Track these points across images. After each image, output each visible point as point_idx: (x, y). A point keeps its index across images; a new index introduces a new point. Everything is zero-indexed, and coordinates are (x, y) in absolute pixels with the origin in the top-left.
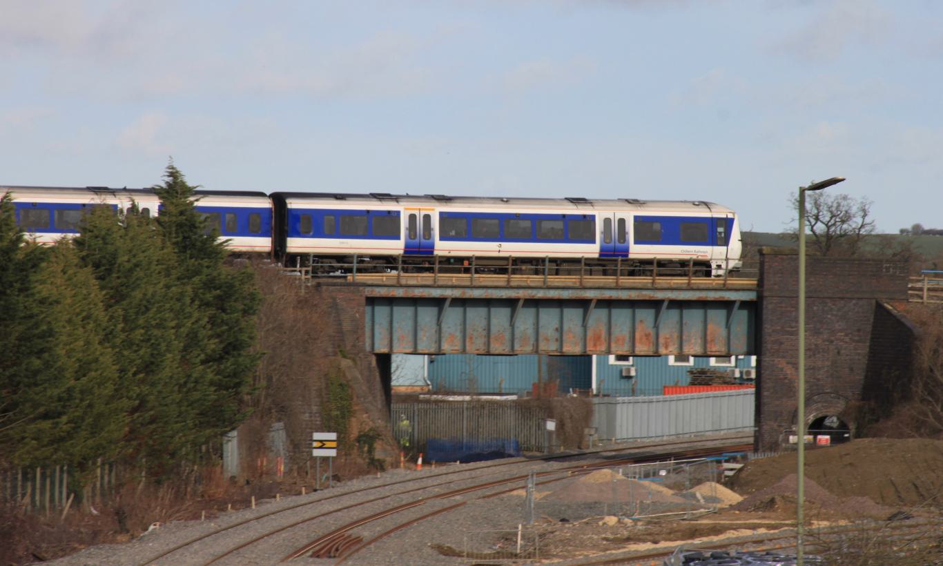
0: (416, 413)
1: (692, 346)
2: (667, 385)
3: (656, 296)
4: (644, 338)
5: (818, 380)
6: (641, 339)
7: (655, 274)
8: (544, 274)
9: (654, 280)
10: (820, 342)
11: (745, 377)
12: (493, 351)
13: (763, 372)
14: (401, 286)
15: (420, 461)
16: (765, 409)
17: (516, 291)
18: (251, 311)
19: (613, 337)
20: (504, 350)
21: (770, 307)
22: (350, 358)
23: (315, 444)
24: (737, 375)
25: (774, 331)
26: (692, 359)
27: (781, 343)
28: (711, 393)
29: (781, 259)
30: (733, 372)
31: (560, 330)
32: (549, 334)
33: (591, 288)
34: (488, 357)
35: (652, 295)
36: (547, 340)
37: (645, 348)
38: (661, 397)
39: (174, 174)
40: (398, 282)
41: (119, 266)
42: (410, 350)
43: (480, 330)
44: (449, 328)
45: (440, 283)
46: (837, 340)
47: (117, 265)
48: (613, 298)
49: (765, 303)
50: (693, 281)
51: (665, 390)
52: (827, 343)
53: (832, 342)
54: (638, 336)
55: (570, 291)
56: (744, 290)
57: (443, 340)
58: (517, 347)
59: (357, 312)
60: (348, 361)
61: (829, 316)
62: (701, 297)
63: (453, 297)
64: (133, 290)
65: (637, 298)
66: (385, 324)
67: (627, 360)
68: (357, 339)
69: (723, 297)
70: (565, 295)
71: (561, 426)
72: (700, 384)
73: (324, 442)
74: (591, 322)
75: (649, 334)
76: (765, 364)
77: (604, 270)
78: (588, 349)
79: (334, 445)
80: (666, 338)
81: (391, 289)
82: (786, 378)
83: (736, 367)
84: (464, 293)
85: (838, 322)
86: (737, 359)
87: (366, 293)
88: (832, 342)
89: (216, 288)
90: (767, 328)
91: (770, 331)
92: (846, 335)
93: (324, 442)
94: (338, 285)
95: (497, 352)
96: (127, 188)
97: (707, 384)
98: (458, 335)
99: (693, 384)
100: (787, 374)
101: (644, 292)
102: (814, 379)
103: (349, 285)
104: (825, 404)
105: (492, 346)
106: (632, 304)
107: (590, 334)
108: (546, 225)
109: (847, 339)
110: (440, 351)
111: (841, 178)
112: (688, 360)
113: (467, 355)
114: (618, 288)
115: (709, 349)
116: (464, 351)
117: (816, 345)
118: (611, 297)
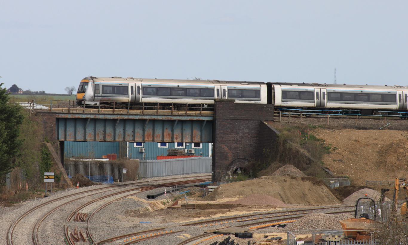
0: (70, 165)
2: (158, 156)
3: (144, 118)
5: (238, 153)
6: (166, 136)
7: (143, 109)
8: (157, 109)
10: (238, 137)
13: (215, 149)
15: (78, 185)
17: (117, 116)
18: (20, 123)
19: (155, 135)
20: (111, 140)
22: (50, 143)
23: (45, 177)
24: (186, 152)
25: (220, 133)
26: (167, 144)
27: (223, 138)
28: (177, 159)
30: (184, 151)
32: (130, 133)
35: (171, 118)
36: (129, 136)
37: (168, 140)
40: (69, 112)
43: (102, 132)
46: (245, 136)
49: (216, 121)
50: (188, 112)
57: (87, 136)
58: (117, 139)
59: (52, 124)
61: (242, 127)
62: (191, 119)
63: (91, 118)
68: (52, 135)
69: (200, 119)
70: (136, 117)
73: (49, 177)
75: (170, 134)
76: (217, 146)
77: (127, 107)
78: (145, 140)
79: (53, 177)
80: (177, 136)
81: (66, 115)
82: (225, 152)
83: (186, 148)
84: (96, 116)
87: (56, 116)
89: (5, 113)
90: (218, 132)
91: (219, 133)
92: (249, 135)
93: (49, 177)
95: (109, 141)
96: (246, 81)
99: (169, 155)
100: (225, 150)
101: (168, 117)
102: (236, 152)
105: (106, 138)
106: (163, 121)
108: (191, 91)
110: (85, 140)
113: (97, 142)
114: (157, 115)
116: (95, 140)
118: (155, 118)
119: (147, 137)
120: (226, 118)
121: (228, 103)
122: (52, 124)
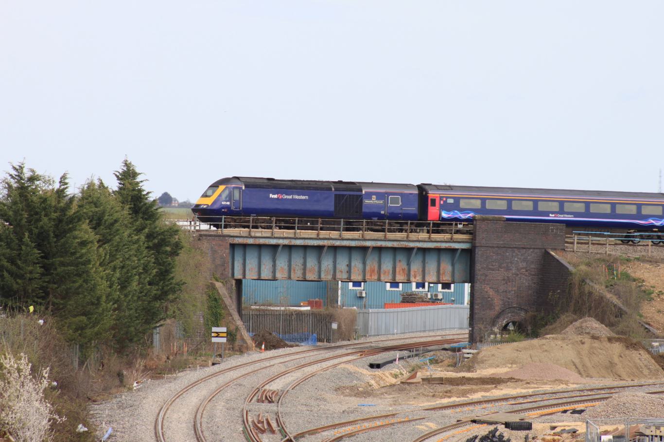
1: (430, 277)
4: (401, 272)
5: (509, 299)
6: (399, 272)
9: (430, 236)
11: (434, 298)
12: (308, 278)
14: (252, 237)
15: (263, 347)
16: (476, 316)
19: (382, 270)
21: (480, 253)
24: (429, 296)
26: (401, 285)
27: (486, 276)
29: (487, 222)
30: (427, 295)
31: (349, 266)
33: (369, 240)
34: (259, 281)
35: (407, 245)
38: (384, 310)
39: (127, 164)
40: (250, 234)
41: (105, 222)
42: (255, 277)
44: (281, 263)
45: (276, 235)
46: (521, 274)
47: (104, 221)
48: (383, 246)
49: (477, 250)
50: (432, 236)
51: (386, 306)
52: (514, 276)
53: (518, 275)
54: (397, 270)
55: (356, 242)
56: (463, 242)
58: (323, 276)
60: (220, 283)
61: (516, 259)
63: (284, 244)
64: (115, 236)
65: (397, 246)
66: (241, 261)
67: (360, 286)
68: (224, 269)
70: (353, 244)
71: (339, 327)
72: (408, 302)
74: (368, 262)
80: (415, 272)
81: (245, 239)
82: (489, 297)
83: (428, 291)
85: (521, 263)
86: (429, 287)
88: (518, 275)
90: (478, 266)
92: (527, 271)
94: (213, 236)
95: (310, 279)
97: (412, 302)
98: (286, 267)
101: (402, 243)
102: (507, 298)
103: (220, 236)
104: (513, 314)
107: (368, 268)
109: (527, 273)
111: (114, 175)
112: (398, 287)
115: (441, 279)
116: (290, 278)
117: (508, 277)
119: (369, 274)
120: (491, 245)
121: (495, 222)
122: (225, 253)
